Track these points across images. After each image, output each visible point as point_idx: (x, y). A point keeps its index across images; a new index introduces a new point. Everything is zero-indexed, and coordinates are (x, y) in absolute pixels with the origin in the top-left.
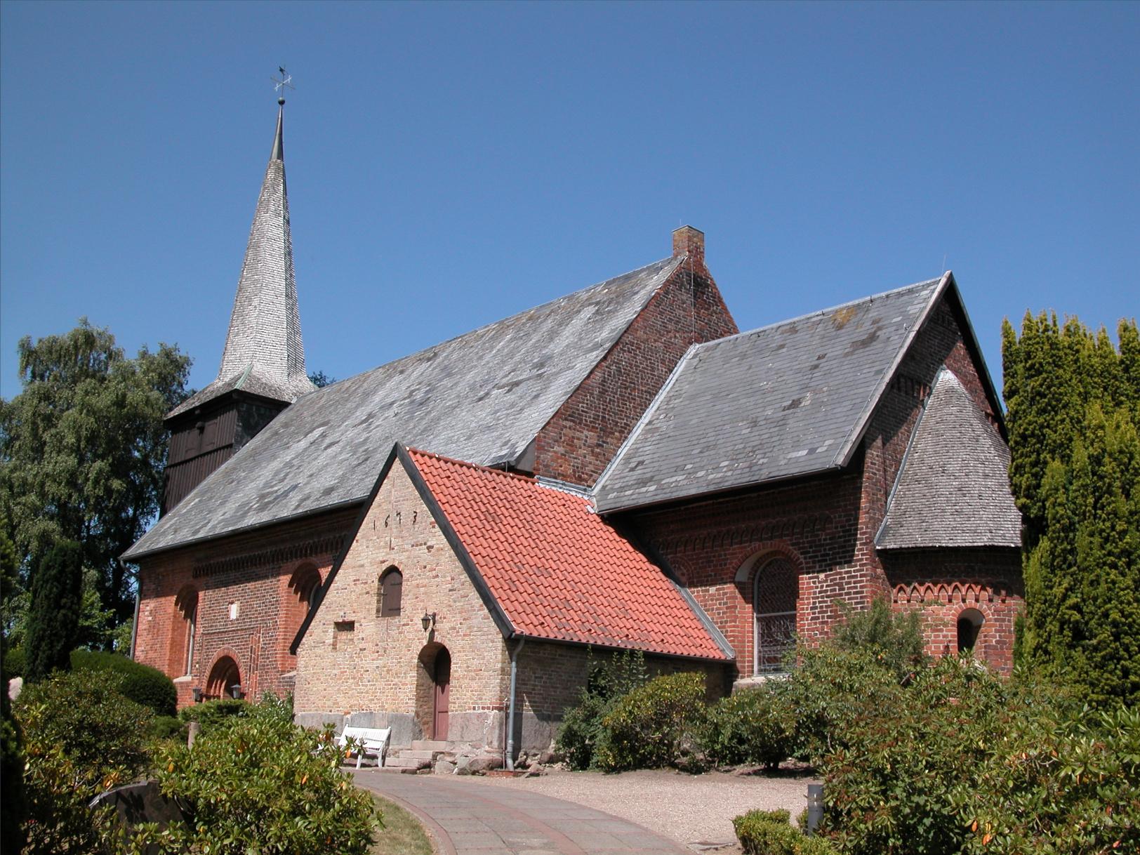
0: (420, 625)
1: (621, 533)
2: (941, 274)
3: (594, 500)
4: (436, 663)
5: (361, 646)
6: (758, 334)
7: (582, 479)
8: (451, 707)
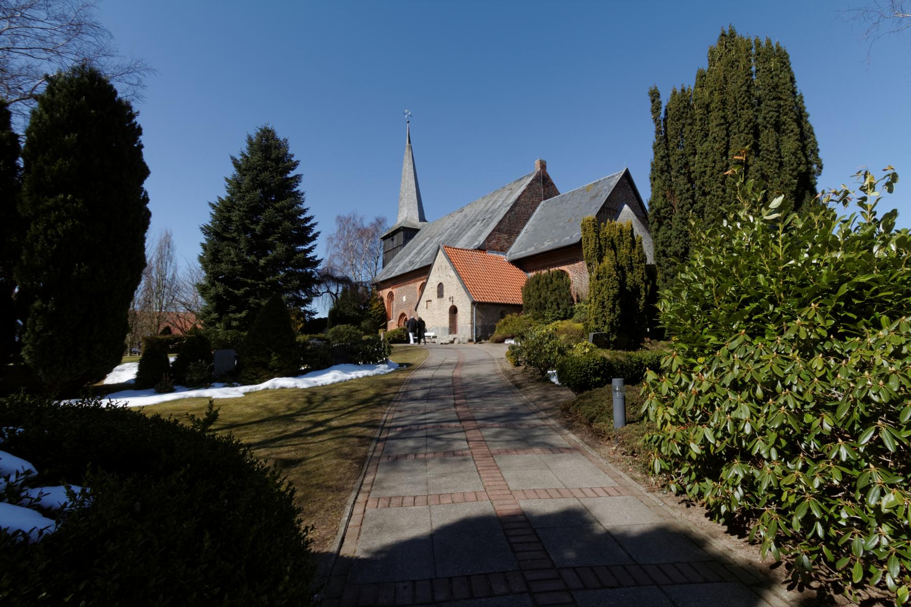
4: (454, 311)
7: (503, 250)
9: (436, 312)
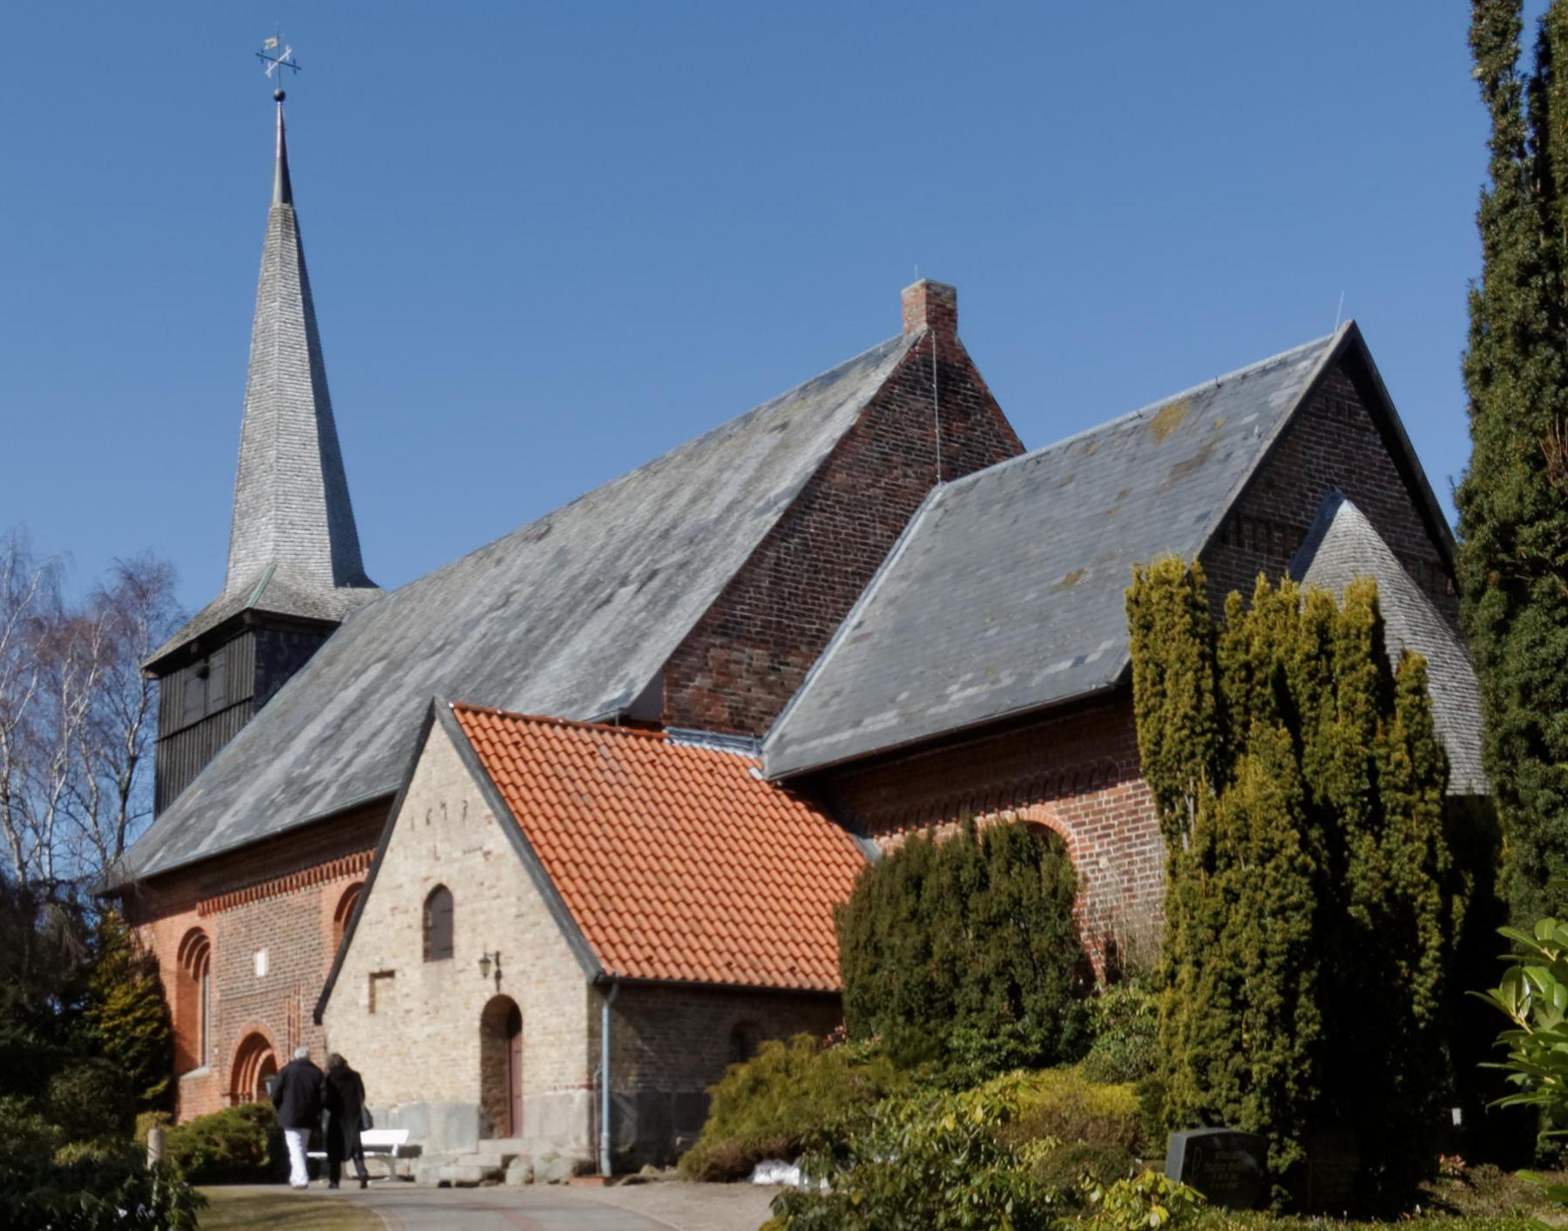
4: (503, 1021)
5: (407, 1006)
7: (746, 725)
9: (417, 1030)
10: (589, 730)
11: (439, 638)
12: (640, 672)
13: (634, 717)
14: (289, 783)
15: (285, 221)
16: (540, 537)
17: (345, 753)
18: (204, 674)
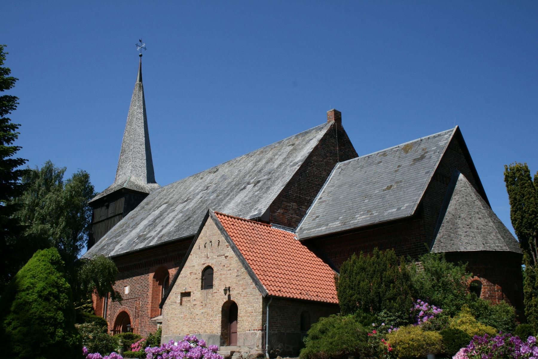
0: (223, 292)
1: (310, 249)
2: (453, 127)
3: (297, 234)
4: (230, 312)
5: (194, 303)
6: (369, 157)
7: (292, 225)
8: (238, 330)
9: (198, 310)
10: (248, 222)
11: (185, 198)
12: (263, 207)
13: (262, 219)
14: (139, 237)
15: (140, 86)
16: (215, 172)
17: (158, 228)
18: (108, 207)
